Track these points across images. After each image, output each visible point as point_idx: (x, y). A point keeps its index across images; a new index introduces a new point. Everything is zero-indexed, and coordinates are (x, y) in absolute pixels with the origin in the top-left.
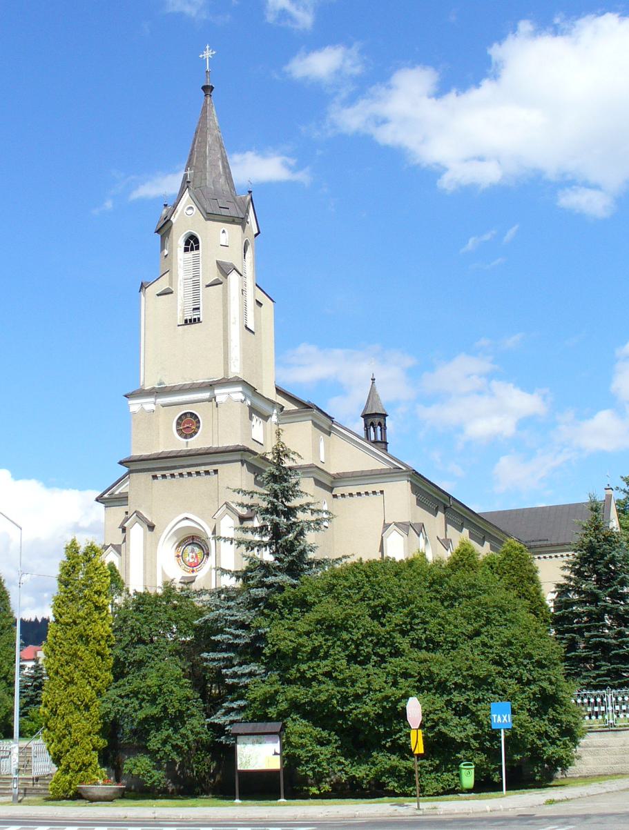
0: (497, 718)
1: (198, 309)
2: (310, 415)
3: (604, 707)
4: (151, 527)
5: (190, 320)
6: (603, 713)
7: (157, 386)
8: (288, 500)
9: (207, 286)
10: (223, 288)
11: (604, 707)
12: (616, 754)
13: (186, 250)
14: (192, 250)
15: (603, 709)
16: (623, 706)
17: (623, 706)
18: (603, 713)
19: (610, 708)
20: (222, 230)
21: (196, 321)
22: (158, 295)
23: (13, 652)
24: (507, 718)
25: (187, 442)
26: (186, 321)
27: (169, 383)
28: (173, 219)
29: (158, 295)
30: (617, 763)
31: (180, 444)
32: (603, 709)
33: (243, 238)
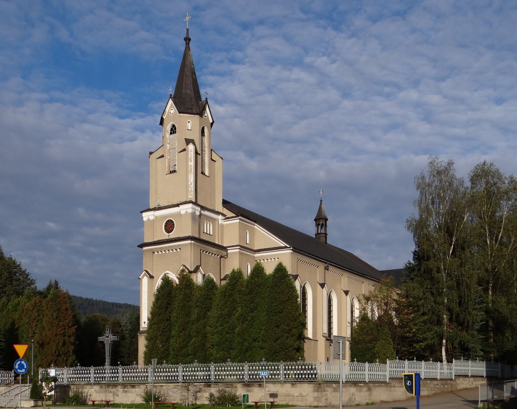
0: (262, 373)
1: (176, 165)
2: (238, 219)
3: (316, 371)
4: (151, 277)
5: (173, 171)
6: (278, 375)
7: (157, 207)
8: (482, 288)
9: (179, 152)
10: (187, 152)
11: (286, 371)
12: (282, 396)
13: (171, 133)
14: (174, 133)
15: (278, 372)
16: (308, 371)
17: (308, 371)
18: (278, 375)
19: (281, 372)
20: (188, 121)
21: (175, 171)
22: (157, 158)
23: (134, 337)
24: (266, 373)
25: (169, 235)
26: (171, 172)
27: (162, 205)
28: (164, 117)
29: (157, 158)
30: (282, 401)
31: (166, 236)
32: (278, 372)
33: (200, 125)
